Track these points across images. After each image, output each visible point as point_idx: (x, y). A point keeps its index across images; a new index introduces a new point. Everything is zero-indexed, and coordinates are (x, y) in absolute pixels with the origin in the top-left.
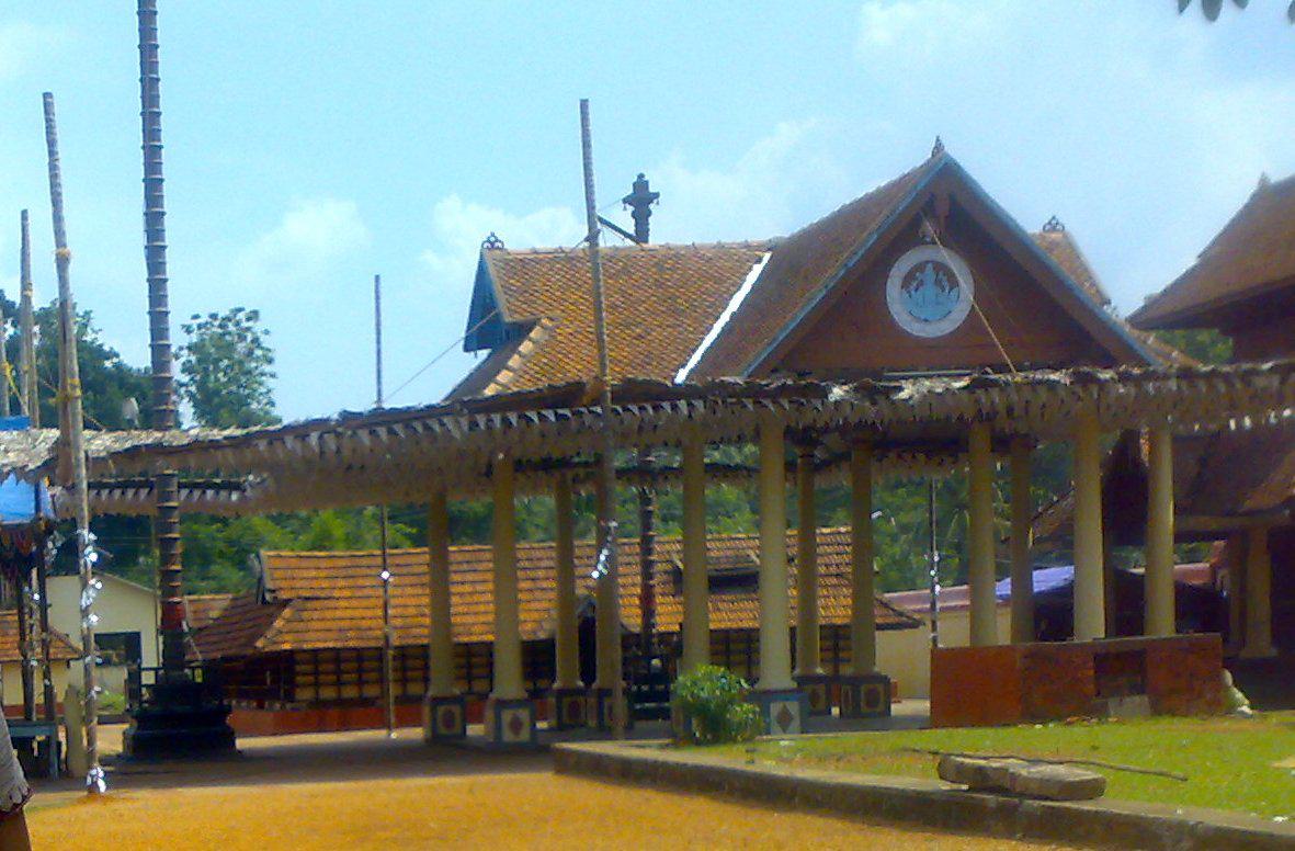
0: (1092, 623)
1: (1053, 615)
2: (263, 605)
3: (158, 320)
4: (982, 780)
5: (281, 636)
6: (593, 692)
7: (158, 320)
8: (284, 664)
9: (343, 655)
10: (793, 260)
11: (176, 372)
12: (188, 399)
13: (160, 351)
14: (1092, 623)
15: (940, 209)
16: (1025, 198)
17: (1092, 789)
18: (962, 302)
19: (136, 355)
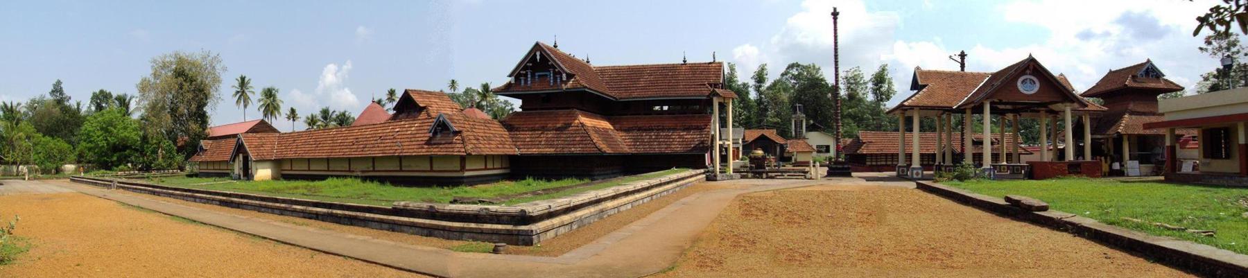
0: (1070, 156)
1: (1061, 154)
2: (858, 143)
3: (837, 75)
4: (1016, 203)
5: (864, 150)
6: (940, 169)
7: (837, 75)
8: (863, 157)
9: (586, 221)
10: (995, 76)
11: (841, 86)
12: (84, 110)
13: (837, 81)
14: (1070, 156)
15: (1031, 67)
16: (1053, 64)
17: (1045, 209)
18: (1036, 88)
19: (830, 81)
